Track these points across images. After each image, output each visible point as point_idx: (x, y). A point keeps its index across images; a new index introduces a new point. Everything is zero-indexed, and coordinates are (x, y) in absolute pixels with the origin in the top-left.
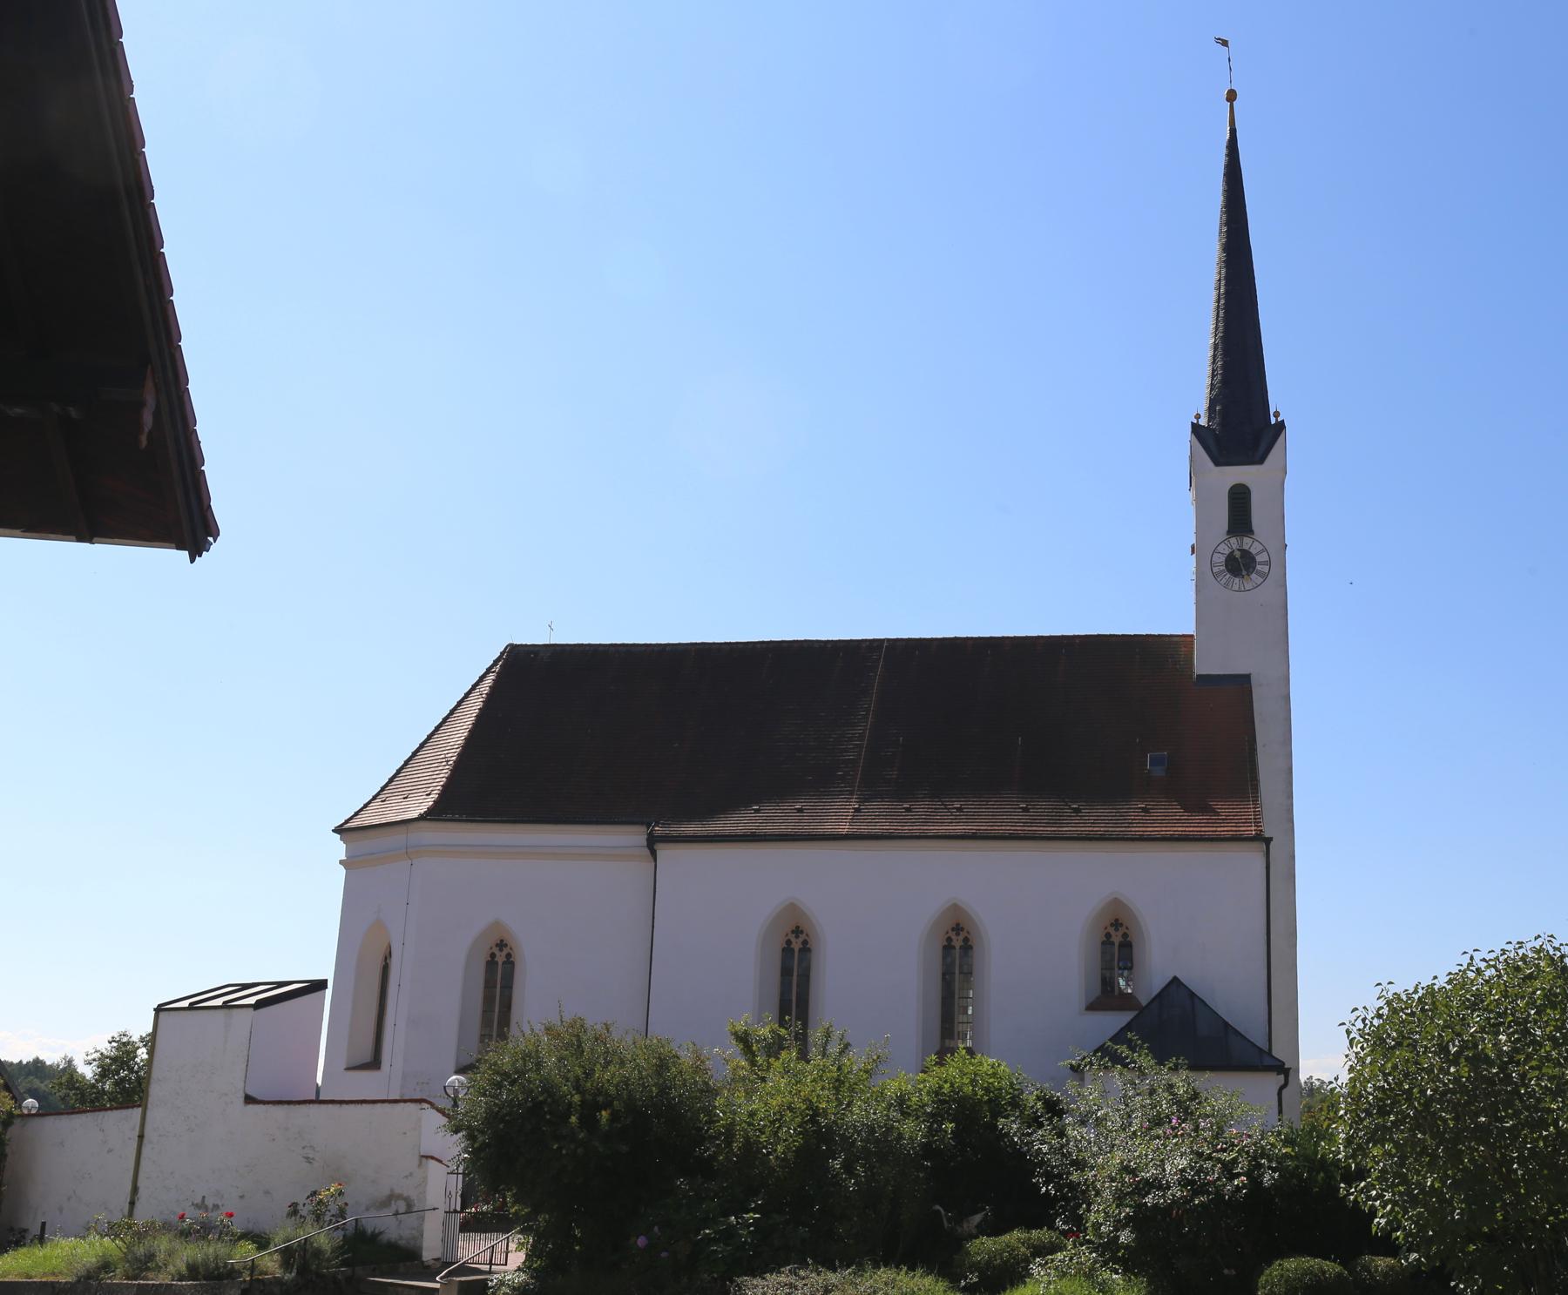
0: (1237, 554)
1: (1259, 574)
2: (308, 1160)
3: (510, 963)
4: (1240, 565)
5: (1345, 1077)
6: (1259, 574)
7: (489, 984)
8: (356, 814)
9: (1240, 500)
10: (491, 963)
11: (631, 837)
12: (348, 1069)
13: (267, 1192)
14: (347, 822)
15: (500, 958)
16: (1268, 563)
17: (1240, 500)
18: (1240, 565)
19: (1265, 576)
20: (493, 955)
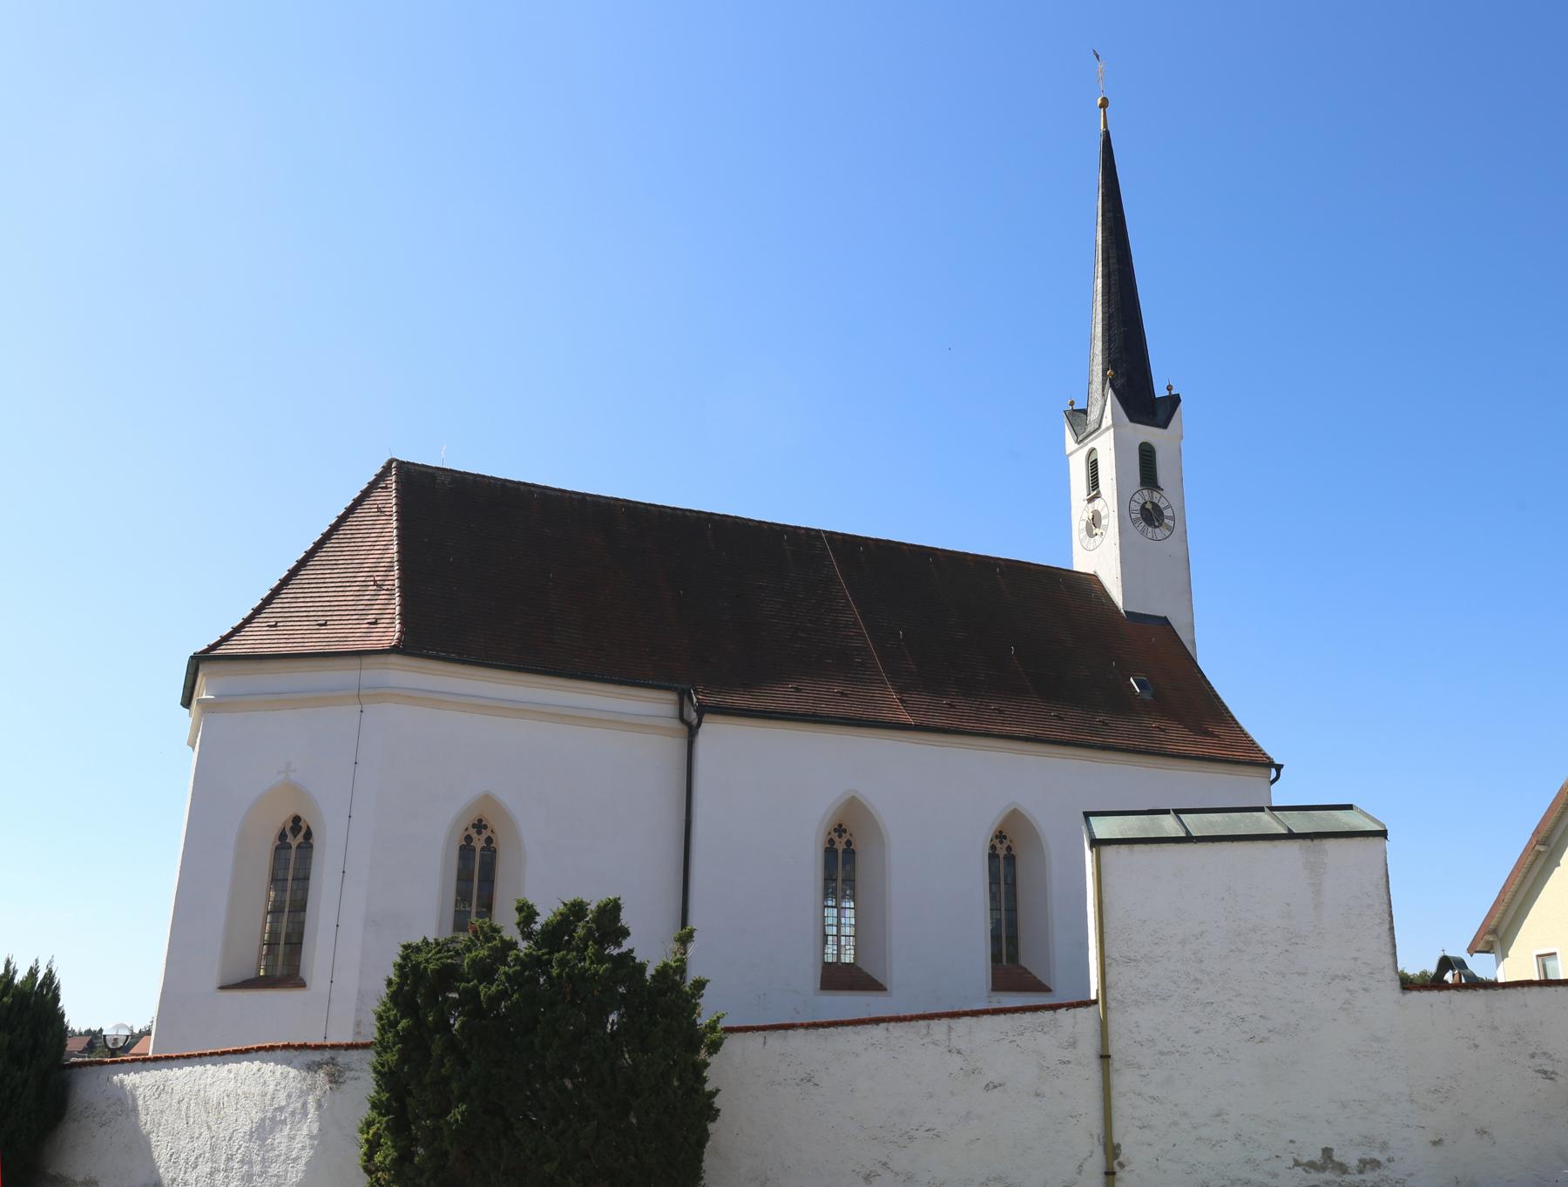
0: (1149, 506)
1: (1168, 528)
2: (1548, 1075)
3: (490, 852)
4: (1151, 516)
5: (377, 1035)
6: (1168, 528)
7: (464, 876)
8: (237, 630)
9: (1147, 455)
10: (466, 851)
11: (655, 705)
12: (222, 988)
13: (1482, 1132)
14: (225, 639)
15: (479, 843)
16: (1173, 518)
17: (1147, 455)
18: (1151, 516)
19: (1171, 530)
20: (468, 838)
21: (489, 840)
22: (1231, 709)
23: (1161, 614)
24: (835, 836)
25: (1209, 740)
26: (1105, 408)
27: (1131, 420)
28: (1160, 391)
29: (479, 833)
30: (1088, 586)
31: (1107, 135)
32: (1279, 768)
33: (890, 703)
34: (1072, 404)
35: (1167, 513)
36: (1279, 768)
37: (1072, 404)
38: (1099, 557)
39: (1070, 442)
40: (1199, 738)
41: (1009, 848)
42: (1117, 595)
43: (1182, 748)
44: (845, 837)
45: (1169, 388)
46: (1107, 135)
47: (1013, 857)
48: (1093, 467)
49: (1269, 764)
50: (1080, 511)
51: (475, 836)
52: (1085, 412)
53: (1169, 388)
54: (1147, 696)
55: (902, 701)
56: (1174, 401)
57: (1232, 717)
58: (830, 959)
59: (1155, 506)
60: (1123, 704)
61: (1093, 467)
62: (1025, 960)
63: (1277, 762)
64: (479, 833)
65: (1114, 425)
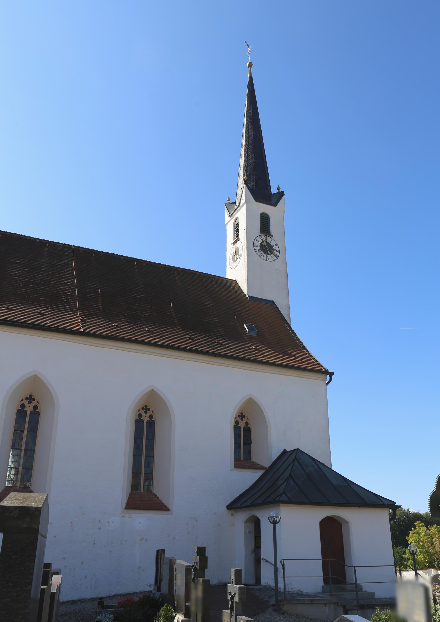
0: (265, 244)
1: (275, 255)
4: (266, 249)
6: (275, 255)
9: (265, 220)
16: (279, 251)
17: (265, 220)
18: (266, 249)
19: (278, 257)
21: (36, 407)
22: (304, 344)
23: (271, 300)
24: (239, 419)
25: (288, 357)
26: (242, 192)
27: (256, 200)
28: (274, 190)
29: (146, 412)
30: (231, 286)
31: (251, 81)
32: (331, 374)
33: (76, 322)
34: (229, 200)
35: (275, 248)
36: (331, 374)
37: (229, 200)
38: (237, 272)
39: (227, 214)
40: (281, 356)
41: (247, 423)
42: (244, 288)
43: (269, 360)
44: (245, 420)
45: (279, 189)
46: (251, 81)
47: (154, 422)
48: (237, 227)
49: (325, 372)
50: (230, 249)
51: (27, 404)
52: (235, 203)
53: (279, 189)
54: (253, 334)
55: (82, 321)
56: (281, 195)
57: (306, 349)
58: (6, 485)
59: (268, 244)
60: (237, 336)
61: (237, 227)
62: (157, 489)
63: (330, 370)
64: (146, 412)
65: (246, 202)
